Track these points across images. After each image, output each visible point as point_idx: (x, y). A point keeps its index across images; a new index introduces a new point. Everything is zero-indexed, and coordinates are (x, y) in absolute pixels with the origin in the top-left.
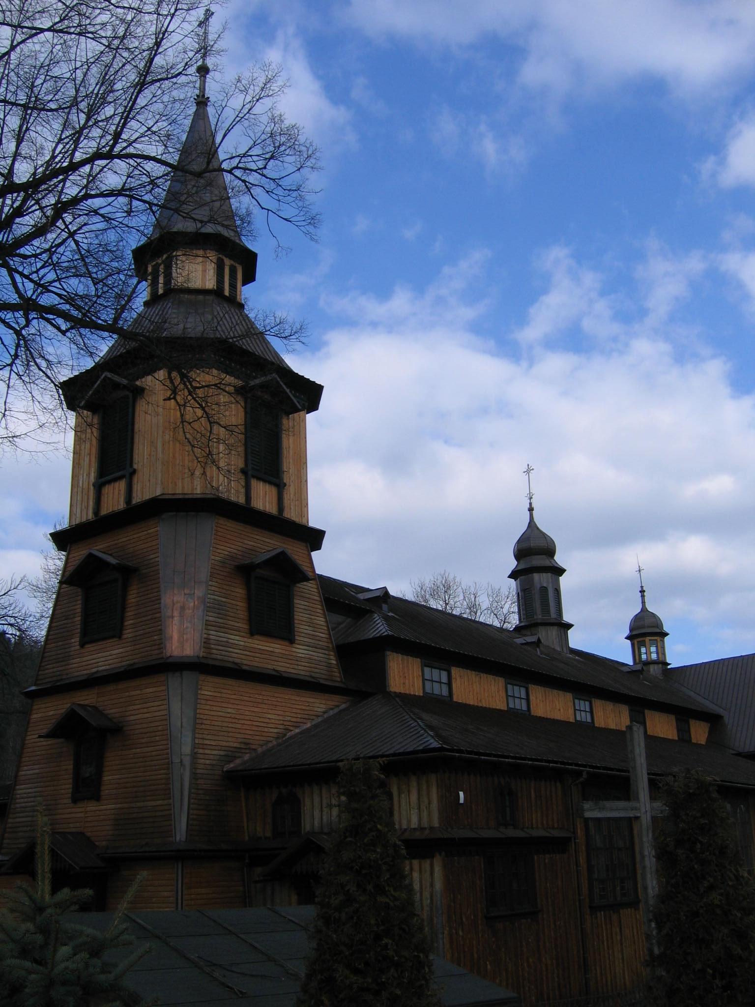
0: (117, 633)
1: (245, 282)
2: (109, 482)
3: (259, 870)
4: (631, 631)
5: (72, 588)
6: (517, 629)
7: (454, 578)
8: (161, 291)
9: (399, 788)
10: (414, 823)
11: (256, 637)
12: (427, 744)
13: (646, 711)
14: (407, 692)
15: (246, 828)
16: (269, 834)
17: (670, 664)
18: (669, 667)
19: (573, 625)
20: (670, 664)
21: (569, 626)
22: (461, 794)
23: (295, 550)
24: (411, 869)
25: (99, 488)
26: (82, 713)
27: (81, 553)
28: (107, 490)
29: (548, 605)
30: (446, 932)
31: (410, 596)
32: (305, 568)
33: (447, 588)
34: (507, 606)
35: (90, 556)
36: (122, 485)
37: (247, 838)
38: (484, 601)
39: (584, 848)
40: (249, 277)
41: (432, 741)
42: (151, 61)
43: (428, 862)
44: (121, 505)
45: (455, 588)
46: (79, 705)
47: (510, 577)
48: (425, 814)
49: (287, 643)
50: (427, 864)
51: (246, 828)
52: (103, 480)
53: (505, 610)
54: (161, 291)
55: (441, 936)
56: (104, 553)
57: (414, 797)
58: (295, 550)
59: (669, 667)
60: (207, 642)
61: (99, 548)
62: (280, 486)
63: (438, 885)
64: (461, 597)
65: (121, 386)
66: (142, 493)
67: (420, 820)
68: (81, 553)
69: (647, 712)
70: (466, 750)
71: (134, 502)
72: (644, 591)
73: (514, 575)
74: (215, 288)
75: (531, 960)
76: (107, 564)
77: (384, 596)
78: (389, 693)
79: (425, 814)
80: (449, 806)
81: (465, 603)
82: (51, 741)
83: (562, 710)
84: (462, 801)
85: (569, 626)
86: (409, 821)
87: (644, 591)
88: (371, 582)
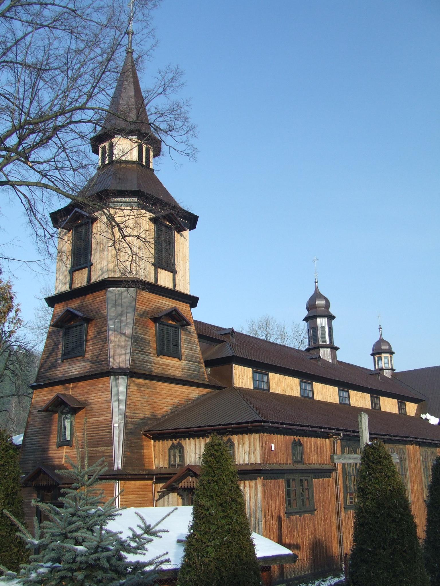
0: (82, 354)
1: (154, 156)
2: (78, 270)
3: (161, 485)
4: (373, 350)
5: (57, 328)
6: (307, 350)
7: (272, 319)
8: (107, 162)
9: (239, 442)
10: (247, 461)
11: (160, 356)
12: (254, 418)
13: (380, 397)
14: (244, 387)
15: (154, 462)
16: (167, 465)
17: (17, 583)
18: (395, 371)
19: (339, 348)
20: (17, 583)
21: (337, 349)
22: (273, 445)
23: (182, 307)
24: (245, 486)
25: (72, 272)
26: (62, 397)
27: (60, 309)
28: (77, 274)
29: (325, 337)
30: (263, 521)
31: (246, 331)
32: (187, 317)
33: (268, 324)
34: (303, 335)
35: (68, 311)
36: (85, 271)
37: (154, 468)
38: (289, 332)
39: (341, 475)
40: (157, 154)
41: (257, 416)
42: (112, 57)
43: (254, 482)
44: (85, 283)
45: (273, 324)
46: (62, 394)
47: (304, 320)
48: (252, 456)
49: (178, 360)
50: (253, 483)
51: (154, 462)
52: (74, 269)
53: (302, 337)
54: (107, 162)
55: (260, 523)
56: (76, 310)
57: (247, 446)
58: (182, 307)
59: (395, 371)
60: (133, 361)
61: (74, 305)
62: (174, 272)
63: (260, 495)
64: (276, 329)
65: (85, 217)
66: (96, 277)
67: (250, 459)
68: (60, 309)
69: (381, 398)
70: (276, 422)
71: (92, 281)
72: (381, 328)
73: (306, 319)
74: (138, 160)
75: (310, 536)
76: (77, 316)
77: (231, 332)
78: (234, 388)
79: (252, 456)
80: (266, 451)
81: (278, 333)
82: (44, 414)
83: (332, 397)
84: (273, 449)
85: (337, 349)
86: (244, 460)
87: (381, 328)
88: (226, 325)
